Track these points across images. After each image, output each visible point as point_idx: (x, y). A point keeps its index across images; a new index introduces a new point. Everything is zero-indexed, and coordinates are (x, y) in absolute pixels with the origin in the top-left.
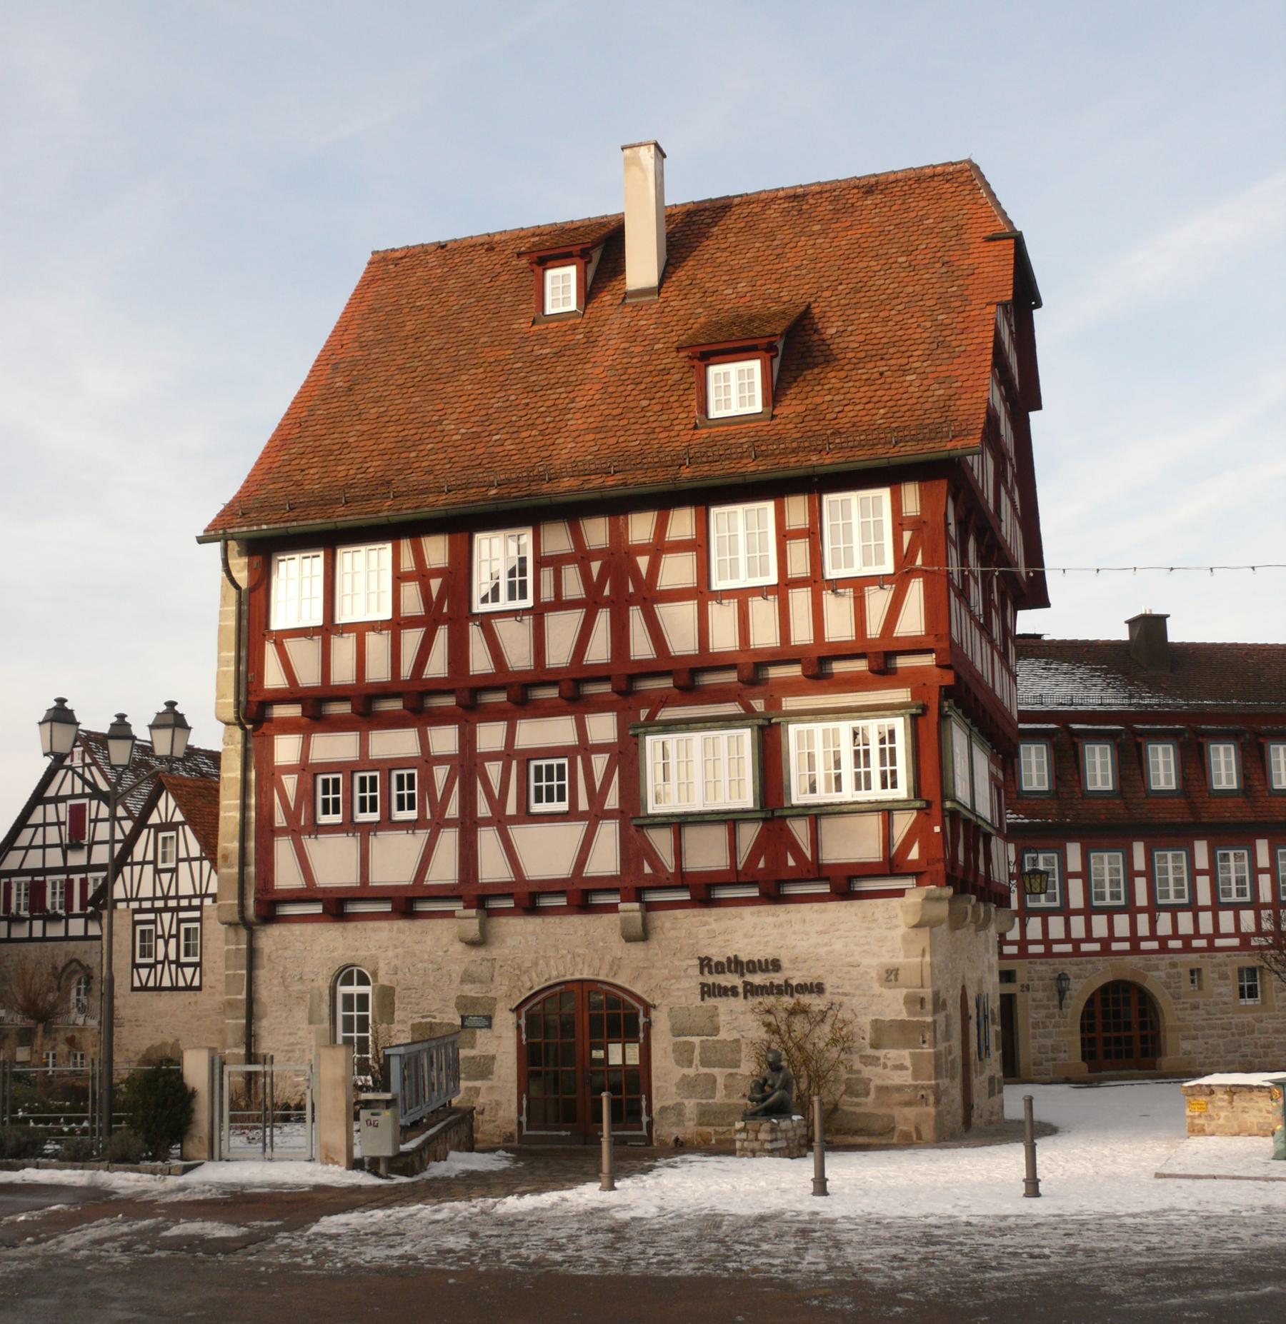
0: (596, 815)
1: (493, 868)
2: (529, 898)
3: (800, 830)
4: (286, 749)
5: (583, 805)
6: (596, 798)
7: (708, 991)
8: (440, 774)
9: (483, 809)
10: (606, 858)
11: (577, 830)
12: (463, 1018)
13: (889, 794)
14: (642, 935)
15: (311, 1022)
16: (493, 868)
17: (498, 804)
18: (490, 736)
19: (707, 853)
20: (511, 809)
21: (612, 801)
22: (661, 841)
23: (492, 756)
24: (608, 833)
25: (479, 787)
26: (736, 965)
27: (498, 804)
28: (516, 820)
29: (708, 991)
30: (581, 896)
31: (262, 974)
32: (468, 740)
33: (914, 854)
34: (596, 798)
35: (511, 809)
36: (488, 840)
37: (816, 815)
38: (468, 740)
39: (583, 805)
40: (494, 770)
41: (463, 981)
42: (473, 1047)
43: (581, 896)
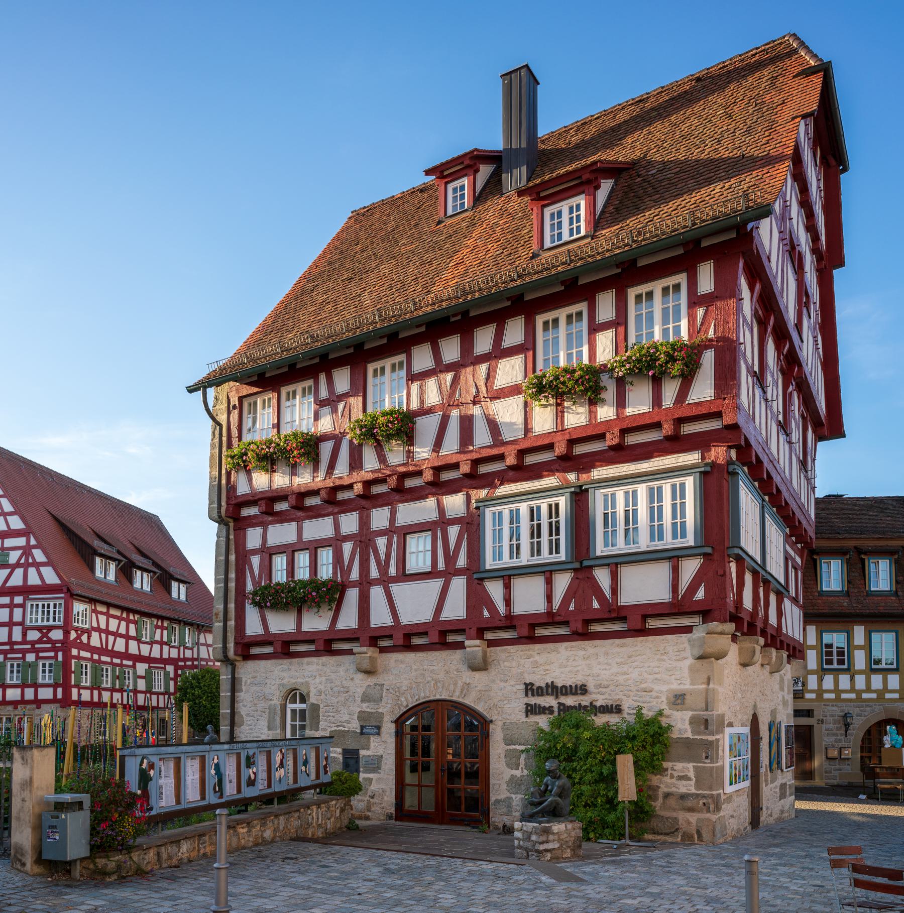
0: (450, 573)
1: (380, 617)
2: (406, 639)
3: (602, 577)
4: (253, 537)
5: (441, 565)
6: (450, 559)
7: (531, 710)
8: (347, 547)
9: (374, 573)
10: (456, 608)
11: (436, 585)
12: (362, 727)
13: (554, 558)
14: (480, 666)
15: (269, 729)
16: (380, 617)
17: (383, 568)
18: (379, 518)
19: (529, 598)
20: (392, 571)
21: (462, 561)
22: (495, 590)
23: (381, 533)
24: (459, 585)
25: (248, 573)
26: (553, 689)
27: (383, 568)
28: (396, 579)
29: (531, 710)
30: (440, 636)
31: (241, 696)
32: (364, 523)
33: (700, 594)
34: (450, 559)
35: (392, 571)
36: (377, 593)
37: (614, 564)
38: (364, 523)
39: (441, 565)
40: (381, 542)
41: (362, 701)
42: (368, 749)
43: (440, 636)
